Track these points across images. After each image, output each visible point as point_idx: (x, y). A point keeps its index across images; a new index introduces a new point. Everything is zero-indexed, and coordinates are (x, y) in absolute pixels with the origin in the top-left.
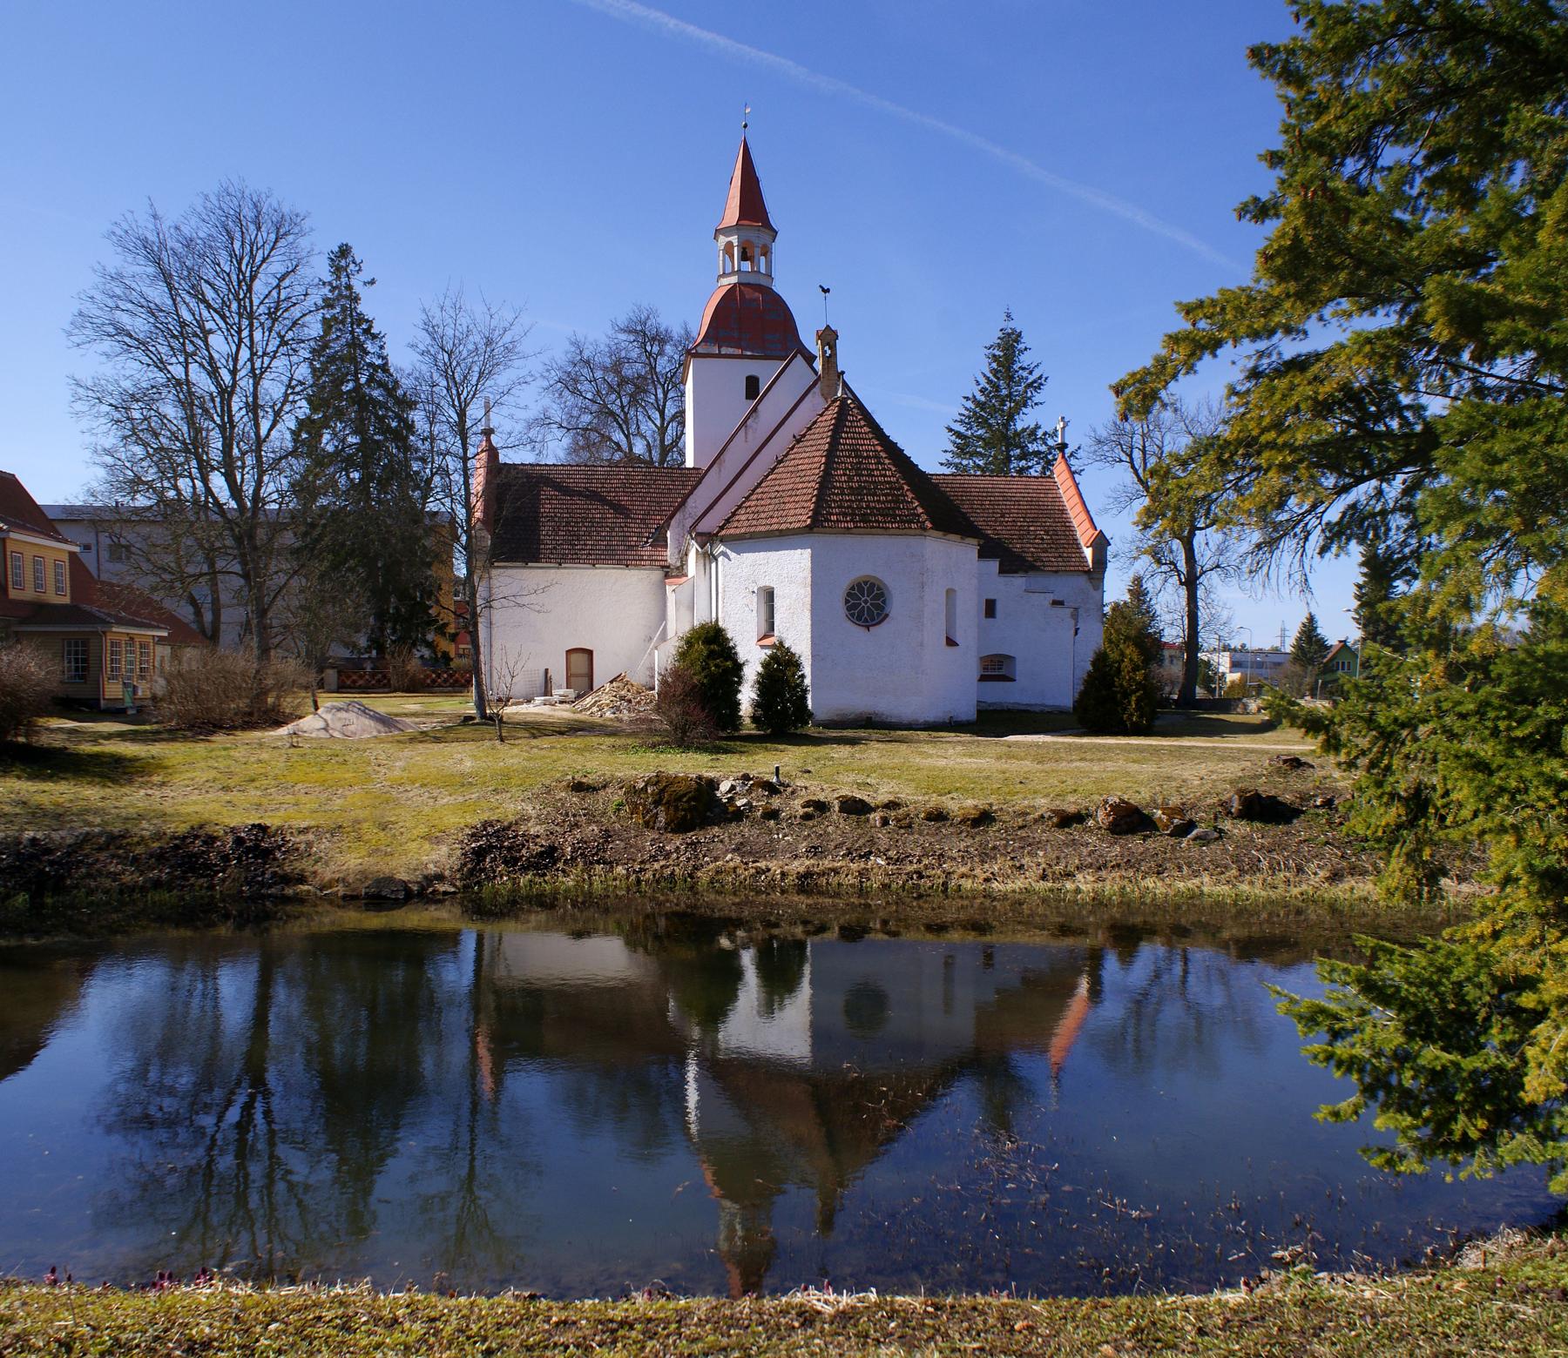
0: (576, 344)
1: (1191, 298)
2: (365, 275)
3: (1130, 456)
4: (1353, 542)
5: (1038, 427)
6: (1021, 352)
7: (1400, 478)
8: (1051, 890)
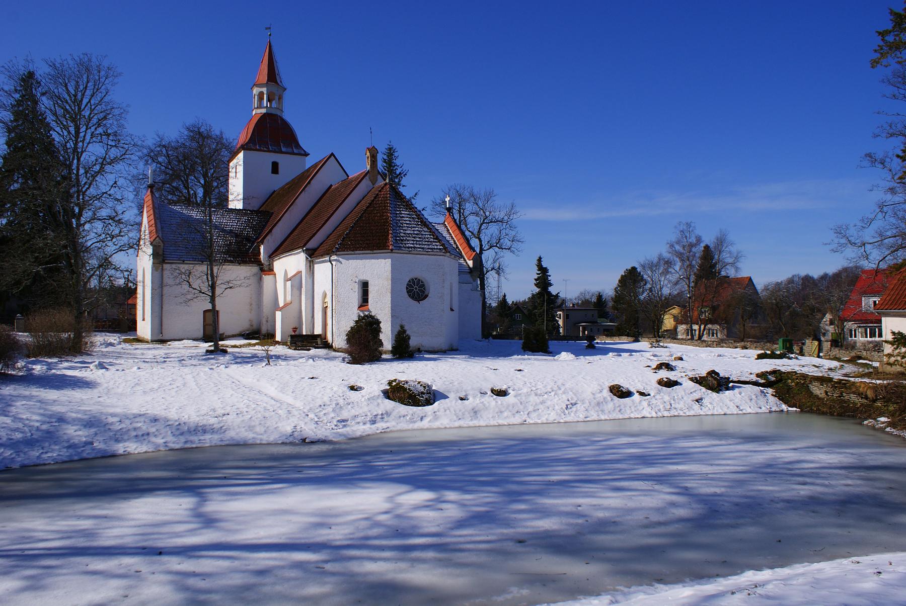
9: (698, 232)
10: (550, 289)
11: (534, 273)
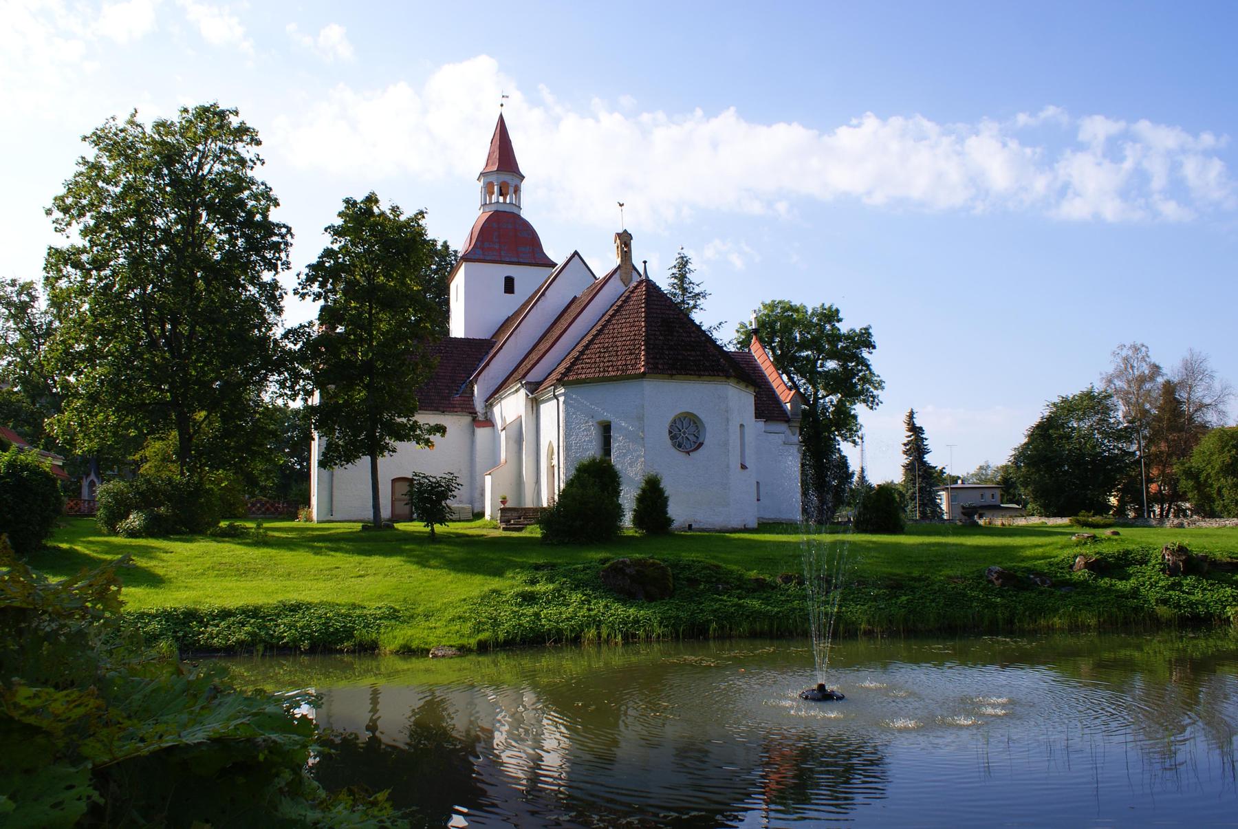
5: (314, 300)
8: (670, 655)
9: (1154, 359)
10: (927, 458)
11: (903, 435)
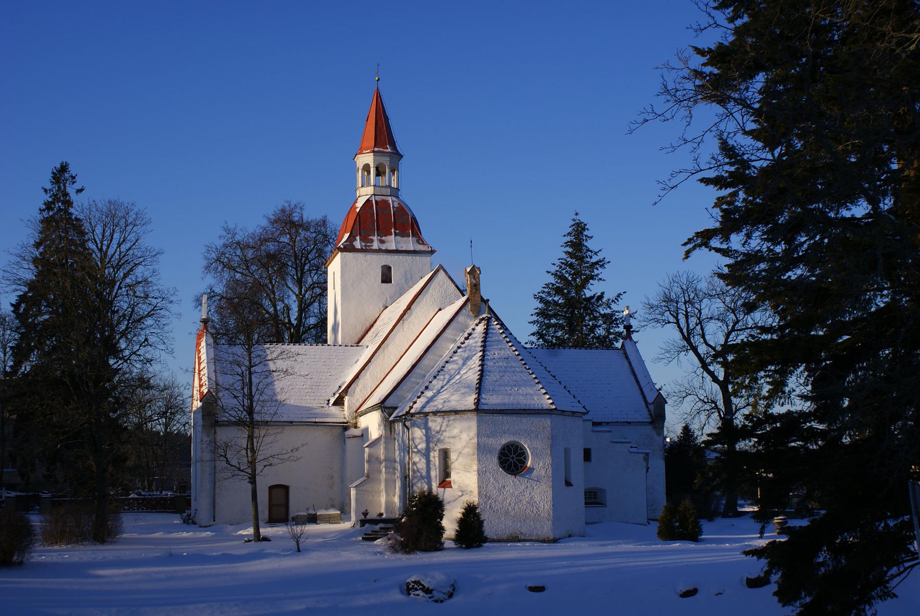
0: (227, 230)
1: (530, 585)
2: (78, 186)
3: (676, 318)
4: (707, 426)
6: (569, 234)
7: (846, 214)
